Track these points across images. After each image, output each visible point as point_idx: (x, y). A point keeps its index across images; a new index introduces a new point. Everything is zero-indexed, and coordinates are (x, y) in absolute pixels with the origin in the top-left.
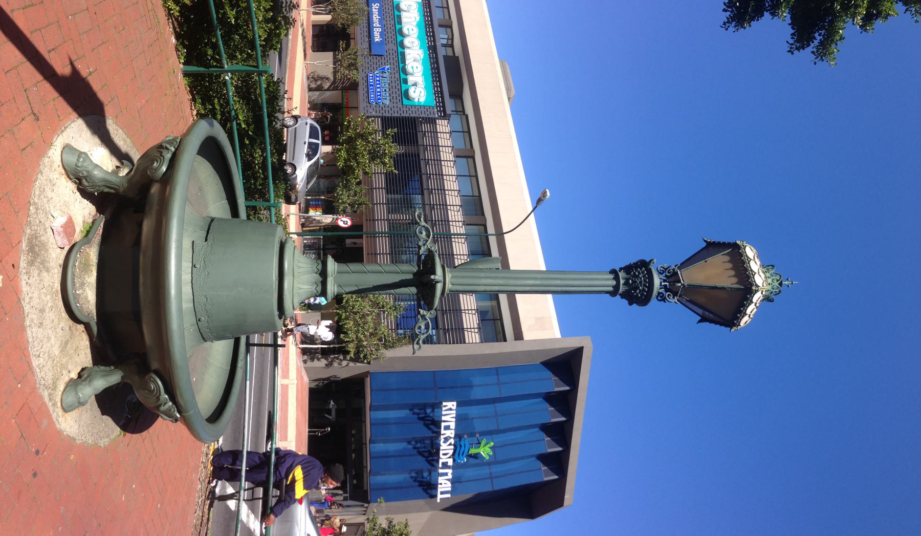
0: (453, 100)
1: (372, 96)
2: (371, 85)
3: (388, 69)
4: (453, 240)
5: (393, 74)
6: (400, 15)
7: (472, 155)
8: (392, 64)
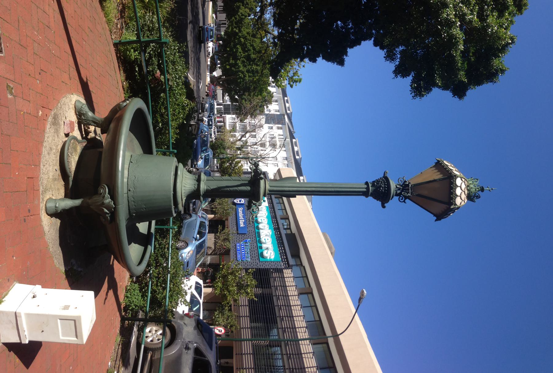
0: (294, 259)
1: (239, 256)
2: (238, 250)
3: (249, 241)
4: (288, 289)
5: (252, 243)
6: (262, 246)
7: (310, 291)
8: (251, 238)
